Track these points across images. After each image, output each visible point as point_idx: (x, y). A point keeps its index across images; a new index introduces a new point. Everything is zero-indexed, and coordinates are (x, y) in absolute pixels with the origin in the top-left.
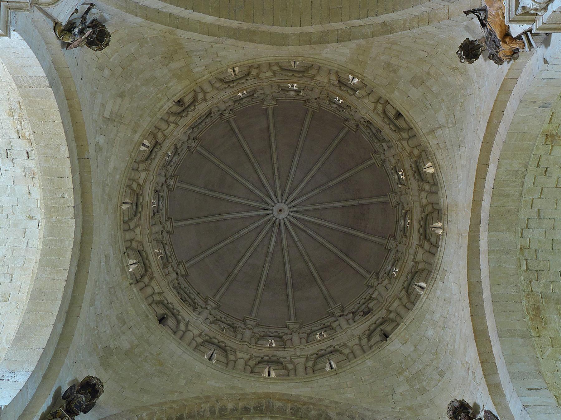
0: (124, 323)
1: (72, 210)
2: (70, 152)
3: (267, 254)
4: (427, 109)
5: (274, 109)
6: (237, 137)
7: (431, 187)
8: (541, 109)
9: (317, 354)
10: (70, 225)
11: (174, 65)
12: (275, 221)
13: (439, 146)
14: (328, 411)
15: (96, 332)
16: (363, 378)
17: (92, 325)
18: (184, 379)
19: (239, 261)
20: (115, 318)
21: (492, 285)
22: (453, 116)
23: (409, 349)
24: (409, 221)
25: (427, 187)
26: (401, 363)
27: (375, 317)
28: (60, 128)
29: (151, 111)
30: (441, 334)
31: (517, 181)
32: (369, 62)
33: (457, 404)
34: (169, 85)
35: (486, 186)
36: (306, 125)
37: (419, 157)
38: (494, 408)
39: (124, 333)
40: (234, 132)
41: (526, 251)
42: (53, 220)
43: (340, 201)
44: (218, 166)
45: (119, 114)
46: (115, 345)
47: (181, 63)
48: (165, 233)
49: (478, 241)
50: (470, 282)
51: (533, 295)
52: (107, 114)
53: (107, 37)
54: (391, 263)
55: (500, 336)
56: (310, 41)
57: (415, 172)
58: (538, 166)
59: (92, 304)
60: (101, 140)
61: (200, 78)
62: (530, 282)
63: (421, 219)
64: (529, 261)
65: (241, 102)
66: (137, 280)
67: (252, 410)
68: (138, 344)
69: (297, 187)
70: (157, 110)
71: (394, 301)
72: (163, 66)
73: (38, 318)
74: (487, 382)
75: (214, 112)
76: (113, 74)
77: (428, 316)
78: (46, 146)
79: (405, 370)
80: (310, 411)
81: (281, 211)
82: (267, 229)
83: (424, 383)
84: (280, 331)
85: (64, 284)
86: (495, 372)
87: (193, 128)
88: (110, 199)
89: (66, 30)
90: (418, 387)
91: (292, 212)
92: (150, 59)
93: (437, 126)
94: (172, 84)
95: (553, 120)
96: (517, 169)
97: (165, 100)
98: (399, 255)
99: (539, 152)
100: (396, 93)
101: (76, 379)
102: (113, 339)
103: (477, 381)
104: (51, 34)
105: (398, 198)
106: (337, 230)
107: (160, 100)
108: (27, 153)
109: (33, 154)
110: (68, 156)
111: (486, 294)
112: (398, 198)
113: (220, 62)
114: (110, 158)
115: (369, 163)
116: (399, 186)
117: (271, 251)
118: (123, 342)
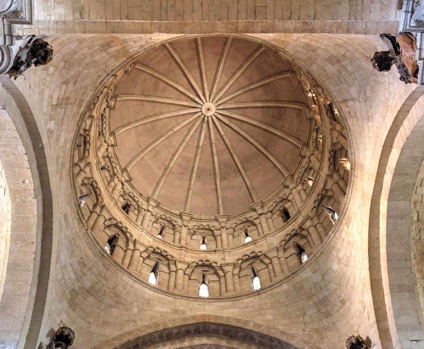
0: (85, 265)
1: (32, 192)
3: (198, 147)
4: (342, 82)
10: (34, 207)
12: (203, 120)
13: (350, 114)
14: (252, 333)
15: (63, 281)
16: (280, 301)
18: (137, 307)
19: (174, 155)
20: (76, 264)
21: (388, 246)
22: (364, 93)
26: (311, 289)
27: (290, 226)
28: (15, 134)
29: (93, 87)
30: (344, 270)
31: (415, 164)
33: (354, 341)
34: (108, 64)
35: (389, 164)
39: (85, 275)
41: (418, 205)
42: (18, 200)
44: (153, 75)
46: (79, 286)
49: (378, 204)
51: (421, 242)
52: (54, 102)
53: (50, 56)
56: (237, 30)
57: (328, 110)
60: (52, 125)
62: (419, 231)
63: (331, 150)
64: (420, 213)
66: (90, 211)
67: (192, 332)
71: (306, 221)
73: (17, 288)
74: (378, 328)
77: (334, 253)
79: (314, 295)
80: (238, 332)
81: (209, 109)
82: (197, 125)
83: (329, 308)
85: (33, 256)
86: (386, 319)
88: (63, 166)
91: (218, 109)
92: (89, 50)
96: (417, 155)
97: (104, 76)
101: (52, 330)
102: (77, 282)
106: (259, 127)
107: (100, 76)
111: (383, 251)
117: (201, 144)
118: (86, 282)
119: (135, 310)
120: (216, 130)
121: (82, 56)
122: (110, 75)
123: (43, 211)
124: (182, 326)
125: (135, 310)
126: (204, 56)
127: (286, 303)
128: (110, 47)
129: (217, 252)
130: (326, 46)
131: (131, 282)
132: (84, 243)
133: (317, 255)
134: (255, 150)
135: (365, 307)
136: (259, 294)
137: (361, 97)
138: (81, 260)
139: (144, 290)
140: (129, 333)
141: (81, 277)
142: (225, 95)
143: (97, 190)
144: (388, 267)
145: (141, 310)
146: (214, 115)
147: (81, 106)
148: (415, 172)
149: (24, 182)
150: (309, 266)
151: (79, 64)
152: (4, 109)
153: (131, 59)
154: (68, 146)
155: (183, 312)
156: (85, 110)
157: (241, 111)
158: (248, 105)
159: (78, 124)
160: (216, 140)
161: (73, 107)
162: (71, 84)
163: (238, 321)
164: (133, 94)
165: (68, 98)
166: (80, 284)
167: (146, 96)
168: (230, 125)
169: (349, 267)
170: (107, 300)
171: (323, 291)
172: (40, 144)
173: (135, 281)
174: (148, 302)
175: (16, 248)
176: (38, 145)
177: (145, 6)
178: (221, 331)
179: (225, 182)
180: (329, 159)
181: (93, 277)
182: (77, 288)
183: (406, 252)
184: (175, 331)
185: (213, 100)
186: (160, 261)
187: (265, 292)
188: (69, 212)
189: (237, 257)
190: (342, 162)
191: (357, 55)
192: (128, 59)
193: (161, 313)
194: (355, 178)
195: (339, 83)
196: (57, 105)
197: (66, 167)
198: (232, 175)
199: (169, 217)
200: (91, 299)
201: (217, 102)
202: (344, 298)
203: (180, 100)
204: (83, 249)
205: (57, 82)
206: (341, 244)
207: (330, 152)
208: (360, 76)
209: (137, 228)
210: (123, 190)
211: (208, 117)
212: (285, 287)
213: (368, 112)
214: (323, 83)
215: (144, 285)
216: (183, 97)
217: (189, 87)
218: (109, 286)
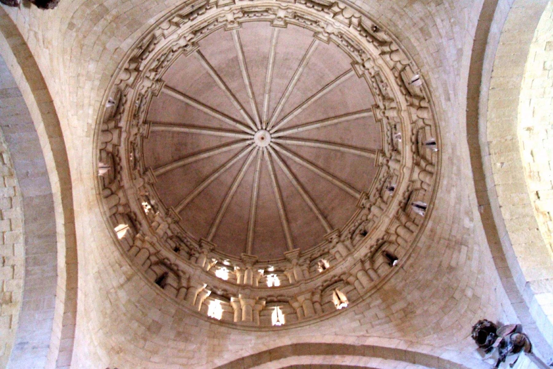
0: (421, 29)
2: (500, 213)
3: (270, 91)
4: (139, 302)
5: (287, 249)
6: (319, 209)
7: (117, 210)
8: (25, 341)
11: (401, 305)
15: (452, 20)
17: (456, 29)
20: (433, 35)
21: (37, 139)
22: (112, 301)
23: (111, 45)
24: (131, 159)
25: (121, 209)
26: (117, 28)
29: (419, 254)
30: (79, 69)
32: (206, 339)
34: (404, 282)
36: (251, 234)
37: (134, 239)
38: (8, 13)
39: (421, 19)
40: (322, 214)
42: (509, 138)
43: (203, 159)
45: (452, 250)
46: (430, 6)
47: (394, 308)
48: (382, 107)
49: (61, 179)
50: (60, 135)
52: (464, 249)
54: (142, 109)
55: (17, 89)
58: (13, 267)
59: (460, 52)
61: (373, 294)
65: (321, 252)
68: (405, 9)
69: (250, 166)
70: (413, 255)
72: (413, 303)
74: (22, 38)
75: (348, 238)
76: (463, 291)
77: (97, 83)
78: (524, 216)
81: (263, 138)
84: (247, 18)
87: (367, 220)
88: (450, 159)
89: (521, 345)
90: (95, 6)
93: (125, 286)
95: (9, 320)
98: (134, 122)
99: (14, 282)
100: (173, 311)
103: (32, 34)
104: (533, 341)
105: (146, 179)
107: (411, 266)
108: (539, 198)
109: (533, 197)
111: (41, 128)
112: (146, 179)
113: (356, 314)
114: (456, 203)
115: (181, 207)
116: (147, 194)
117: (267, 96)
120: (250, 113)
121: (434, 301)
122: (400, 266)
123: (478, 119)
126: (276, 204)
128: (404, 310)
130: (168, 346)
132: (422, 56)
133: (117, 70)
135: (43, 42)
137: (114, 295)
141: (427, 17)
143: (400, 83)
144: (29, 114)
146: (256, 132)
147: (432, 231)
148: (30, 240)
149: (502, 163)
150: (125, 54)
151: (437, 291)
152: (527, 282)
156: (426, 223)
157: (224, 141)
159: (434, 205)
160: (248, 102)
161: (442, 233)
165: (448, 246)
166: (429, 8)
169: (74, 75)
171: (101, 30)
172: (482, 211)
173: (354, 3)
175: (515, 80)
176: (485, 210)
179: (231, 56)
180: (120, 160)
181: (410, 14)
183: (10, 134)
185: (258, 150)
187: (177, 7)
188: (443, 101)
190: (106, 166)
191: (132, 346)
192: (382, 287)
194: (93, 186)
195: (142, 299)
196: (461, 244)
198: (223, 66)
201: (254, 148)
202: (71, 32)
204: (424, 49)
206: (91, 98)
207: (121, 168)
208: (121, 321)
210: (362, 58)
211: (262, 129)
212: (152, 21)
213: (103, 281)
214: (158, 292)
217: (289, 163)
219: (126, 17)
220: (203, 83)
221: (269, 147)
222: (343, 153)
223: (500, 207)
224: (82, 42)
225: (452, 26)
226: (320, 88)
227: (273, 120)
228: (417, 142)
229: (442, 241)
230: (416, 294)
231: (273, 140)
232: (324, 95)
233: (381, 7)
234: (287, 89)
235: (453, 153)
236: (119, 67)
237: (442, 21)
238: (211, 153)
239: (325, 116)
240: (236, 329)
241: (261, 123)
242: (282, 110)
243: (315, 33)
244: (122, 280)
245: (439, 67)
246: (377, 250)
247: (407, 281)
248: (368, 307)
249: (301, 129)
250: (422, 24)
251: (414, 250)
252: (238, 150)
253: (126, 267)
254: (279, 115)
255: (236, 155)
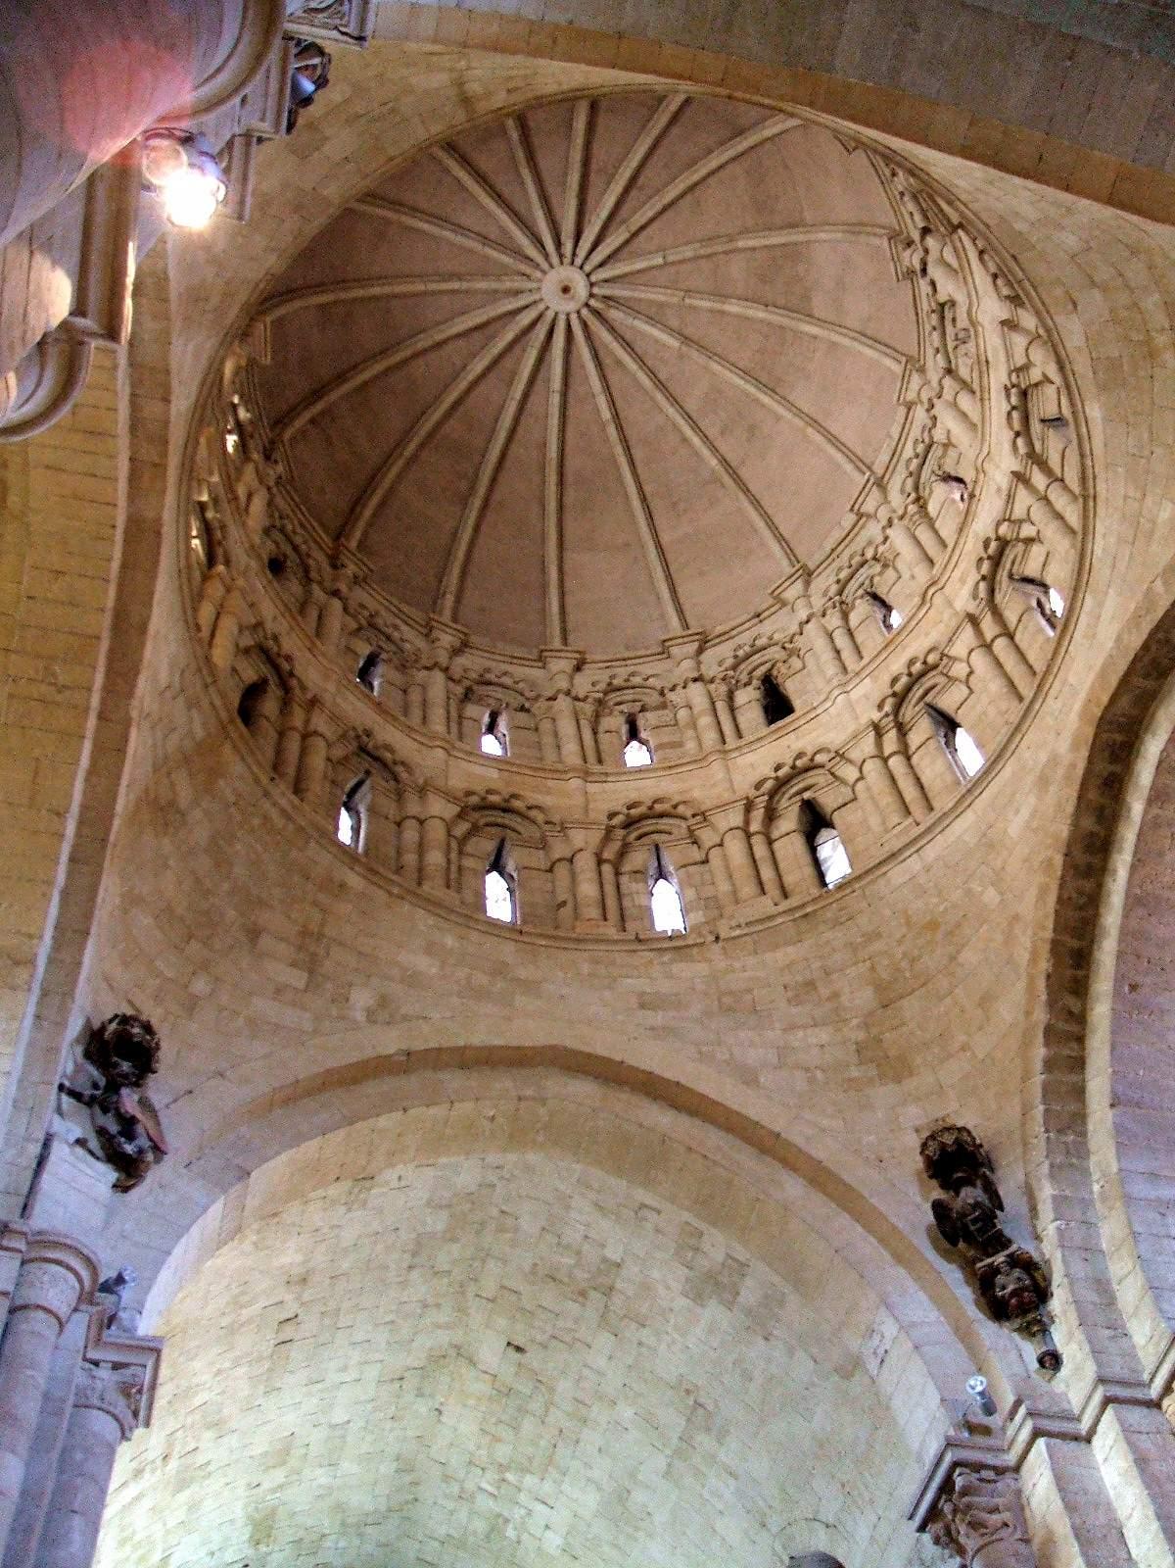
0: (810, 985)
9: (1018, 434)
11: (185, 794)
12: (596, 313)
15: (819, 1074)
16: (1131, 451)
20: (794, 1010)
22: (435, 59)
26: (1128, 339)
39: (836, 995)
47: (181, 779)
52: (298, 979)
70: (291, 827)
76: (205, 966)
81: (566, 290)
94: (228, 792)
110: (398, 1115)
118: (857, 1002)
119: (991, 896)
124: (1080, 798)
125: (991, 896)
127: (1146, 436)
129: (977, 493)
131: (914, 864)
132: (751, 961)
134: (736, 169)
136: (1095, 497)
138: (790, 994)
139: (952, 839)
140: (1034, 959)
142: (494, 295)
145: (997, 881)
147: (342, 885)
153: (230, 728)
154: (450, 941)
155: (1054, 760)
158: (577, 156)
162: (264, 917)
163: (1136, 618)
164: (454, 535)
167: (472, 489)
168: (633, 229)
170: (931, 962)
171: (1142, 305)
174: (989, 843)
177: (37, 752)
178: (1149, 684)
182: (861, 1035)
184: (1089, 823)
186: (928, 699)
187: (1094, 478)
189: (1007, 447)
193: (1028, 826)
196: (311, 972)
197: (509, 960)
198: (801, 269)
199: (851, 557)
200: (911, 1007)
203: (514, 374)
205: (244, 965)
208: (367, 65)
209: (819, 711)
215: (939, 829)
216: (508, 363)
218: (898, 936)
219: (1142, 373)
220: (777, 198)
221: (536, 297)
222: (464, 502)
223: (405, 1110)
224: (1142, 256)
225: (807, 1070)
226: (647, 489)
227: (604, 335)
228: (505, 810)
229: (317, 916)
230: (201, 834)
231: (550, 315)
232: (626, 496)
233: (887, 912)
234: (674, 400)
235: (517, 980)
236: (1027, 284)
237: (822, 1046)
238: (579, 140)
239: (570, 478)
240: (221, 344)
241: (607, 298)
242: (619, 363)
243: (810, 574)
244: (474, 88)
245: (719, 1000)
246: (276, 668)
247: (232, 810)
248: (192, 704)
249: (556, 399)
250: (824, 992)
251: (301, 829)
252: (557, 210)
253: (499, 100)
254: (611, 353)
255: (545, 199)
